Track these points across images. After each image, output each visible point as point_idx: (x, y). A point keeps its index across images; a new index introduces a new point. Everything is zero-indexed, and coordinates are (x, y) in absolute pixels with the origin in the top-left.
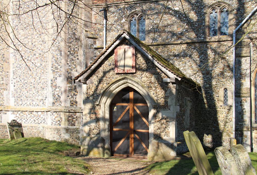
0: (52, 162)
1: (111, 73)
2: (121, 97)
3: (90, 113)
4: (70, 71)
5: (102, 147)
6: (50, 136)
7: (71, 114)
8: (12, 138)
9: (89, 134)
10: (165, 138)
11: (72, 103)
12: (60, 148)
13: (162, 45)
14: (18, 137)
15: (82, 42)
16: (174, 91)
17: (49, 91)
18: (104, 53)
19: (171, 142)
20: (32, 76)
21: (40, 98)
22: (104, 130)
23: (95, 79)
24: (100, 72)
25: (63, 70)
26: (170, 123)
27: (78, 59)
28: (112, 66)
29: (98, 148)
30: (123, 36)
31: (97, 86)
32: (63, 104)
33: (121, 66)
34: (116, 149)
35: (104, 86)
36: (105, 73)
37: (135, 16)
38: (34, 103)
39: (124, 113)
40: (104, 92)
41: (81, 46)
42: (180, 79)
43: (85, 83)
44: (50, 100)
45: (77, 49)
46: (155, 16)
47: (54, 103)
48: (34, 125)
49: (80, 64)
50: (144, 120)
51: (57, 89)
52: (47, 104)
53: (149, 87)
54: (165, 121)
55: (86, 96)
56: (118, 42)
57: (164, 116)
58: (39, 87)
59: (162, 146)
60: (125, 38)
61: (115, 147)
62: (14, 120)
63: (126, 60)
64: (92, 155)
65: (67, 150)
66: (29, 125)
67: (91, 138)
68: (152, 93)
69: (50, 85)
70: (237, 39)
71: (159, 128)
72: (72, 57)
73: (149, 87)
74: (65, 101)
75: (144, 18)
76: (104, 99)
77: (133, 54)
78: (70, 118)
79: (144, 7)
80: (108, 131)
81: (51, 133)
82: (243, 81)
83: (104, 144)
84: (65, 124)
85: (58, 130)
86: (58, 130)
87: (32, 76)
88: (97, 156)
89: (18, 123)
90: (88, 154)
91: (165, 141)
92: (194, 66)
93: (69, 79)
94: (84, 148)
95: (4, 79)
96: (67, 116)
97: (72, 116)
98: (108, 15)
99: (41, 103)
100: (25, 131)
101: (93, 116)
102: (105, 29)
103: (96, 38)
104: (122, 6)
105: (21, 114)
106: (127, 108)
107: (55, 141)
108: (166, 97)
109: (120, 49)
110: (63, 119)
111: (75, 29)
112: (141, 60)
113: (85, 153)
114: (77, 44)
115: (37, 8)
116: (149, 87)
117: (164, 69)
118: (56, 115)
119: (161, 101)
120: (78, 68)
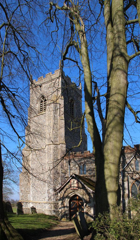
0: (46, 220)
1: (69, 189)
2: (72, 199)
3: (61, 204)
4: (55, 187)
5: (66, 217)
6: (47, 213)
7: (56, 204)
8: (32, 213)
9: (61, 212)
10: (90, 214)
11: (56, 200)
12: (50, 217)
14: (34, 213)
15: (60, 174)
16: (92, 196)
17: (46, 195)
18: (66, 182)
19: (92, 215)
20: (40, 188)
21: (43, 197)
22: (67, 211)
23: (63, 191)
24: (65, 189)
25: (52, 186)
26: (92, 208)
27: (58, 181)
28: (69, 187)
29: (65, 217)
30: (73, 175)
31: (64, 194)
32: (52, 200)
33: (73, 187)
35: (66, 194)
36: (67, 189)
37: (82, 164)
38: (41, 200)
39: (75, 204)
40: (67, 196)
41: (60, 176)
42: (94, 192)
43: (59, 193)
44: (47, 198)
45: (58, 177)
46: (90, 164)
47: (49, 200)
48: (40, 209)
49: (59, 184)
50: (83, 207)
51: (50, 194)
52: (46, 200)
53: (83, 195)
54: (89, 207)
55: (60, 198)
56: (71, 178)
57: (89, 205)
58: (42, 193)
59: (88, 217)
60: (73, 176)
61: (72, 218)
62: (33, 206)
63: (74, 185)
64: (62, 220)
65: (53, 218)
66: (39, 209)
67: (62, 214)
68: (84, 197)
69: (47, 192)
70: (123, 174)
71: (87, 210)
72: (56, 181)
73: (83, 195)
74: (53, 199)
75: (85, 165)
76: (67, 199)
77: (77, 182)
78: (55, 206)
79: (85, 161)
80: (69, 211)
81: (47, 212)
82: (125, 191)
83: (67, 216)
84: (53, 208)
85: (51, 211)
86: (51, 211)
87: (40, 188)
88: (64, 220)
89: (34, 207)
90: (61, 220)
91: (90, 215)
93: (55, 190)
94: (59, 217)
97: (56, 206)
98: (71, 163)
99: (44, 199)
100: (37, 211)
101: (63, 206)
102: (69, 169)
103: (66, 173)
105: (35, 204)
106: (76, 202)
107: (49, 215)
108: (89, 199)
109: (72, 180)
110: (53, 207)
111: (57, 169)
112: (80, 185)
113: (59, 219)
114: (58, 175)
116: (83, 195)
117: (88, 188)
118: (50, 205)
119: (88, 200)
120: (59, 185)
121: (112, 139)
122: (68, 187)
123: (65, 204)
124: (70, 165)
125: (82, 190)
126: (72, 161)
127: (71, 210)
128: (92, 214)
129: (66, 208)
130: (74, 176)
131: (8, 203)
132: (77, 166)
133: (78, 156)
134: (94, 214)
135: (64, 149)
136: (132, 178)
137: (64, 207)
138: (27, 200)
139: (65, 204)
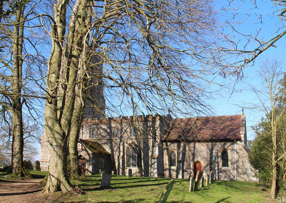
10: (89, 170)
16: (91, 156)
53: (85, 155)
70: (121, 139)
92: (109, 148)
96: (224, 126)
108: (89, 158)
116: (85, 155)
119: (88, 159)
121: (72, 130)
125: (85, 151)
130: (80, 141)
131: (29, 162)
132: (88, 131)
133: (89, 122)
134: (92, 170)
136: (127, 143)
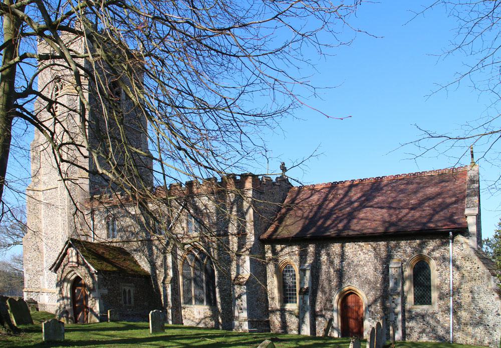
13: (127, 242)
19: (97, 313)
22: (68, 305)
23: (60, 270)
29: (63, 317)
34: (78, 319)
42: (97, 271)
83: (68, 315)
95: (40, 267)
98: (95, 217)
104: (102, 210)
108: (93, 284)
115: (231, 112)
119: (91, 286)
122: (66, 263)
123: (64, 295)
124: (93, 221)
126: (97, 212)
127: (75, 305)
128: (98, 312)
129: (65, 300)
134: (101, 312)
135: (86, 187)
137: (63, 298)
138: (39, 288)
139: (64, 295)
